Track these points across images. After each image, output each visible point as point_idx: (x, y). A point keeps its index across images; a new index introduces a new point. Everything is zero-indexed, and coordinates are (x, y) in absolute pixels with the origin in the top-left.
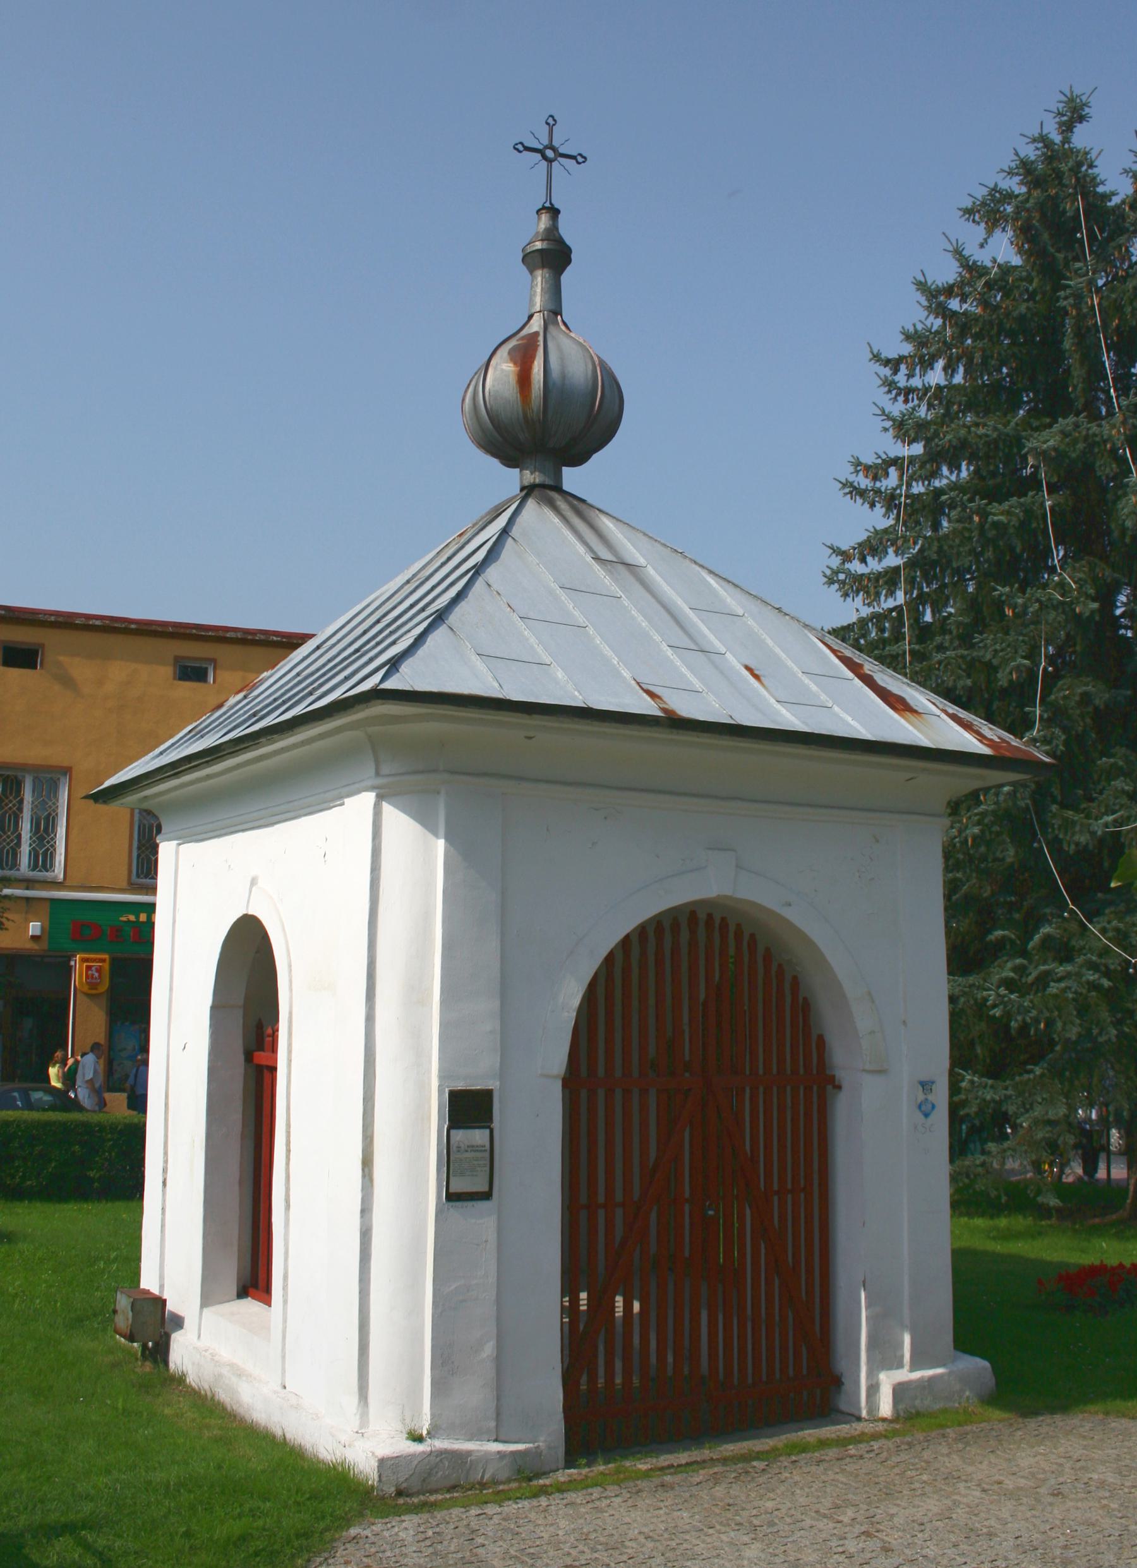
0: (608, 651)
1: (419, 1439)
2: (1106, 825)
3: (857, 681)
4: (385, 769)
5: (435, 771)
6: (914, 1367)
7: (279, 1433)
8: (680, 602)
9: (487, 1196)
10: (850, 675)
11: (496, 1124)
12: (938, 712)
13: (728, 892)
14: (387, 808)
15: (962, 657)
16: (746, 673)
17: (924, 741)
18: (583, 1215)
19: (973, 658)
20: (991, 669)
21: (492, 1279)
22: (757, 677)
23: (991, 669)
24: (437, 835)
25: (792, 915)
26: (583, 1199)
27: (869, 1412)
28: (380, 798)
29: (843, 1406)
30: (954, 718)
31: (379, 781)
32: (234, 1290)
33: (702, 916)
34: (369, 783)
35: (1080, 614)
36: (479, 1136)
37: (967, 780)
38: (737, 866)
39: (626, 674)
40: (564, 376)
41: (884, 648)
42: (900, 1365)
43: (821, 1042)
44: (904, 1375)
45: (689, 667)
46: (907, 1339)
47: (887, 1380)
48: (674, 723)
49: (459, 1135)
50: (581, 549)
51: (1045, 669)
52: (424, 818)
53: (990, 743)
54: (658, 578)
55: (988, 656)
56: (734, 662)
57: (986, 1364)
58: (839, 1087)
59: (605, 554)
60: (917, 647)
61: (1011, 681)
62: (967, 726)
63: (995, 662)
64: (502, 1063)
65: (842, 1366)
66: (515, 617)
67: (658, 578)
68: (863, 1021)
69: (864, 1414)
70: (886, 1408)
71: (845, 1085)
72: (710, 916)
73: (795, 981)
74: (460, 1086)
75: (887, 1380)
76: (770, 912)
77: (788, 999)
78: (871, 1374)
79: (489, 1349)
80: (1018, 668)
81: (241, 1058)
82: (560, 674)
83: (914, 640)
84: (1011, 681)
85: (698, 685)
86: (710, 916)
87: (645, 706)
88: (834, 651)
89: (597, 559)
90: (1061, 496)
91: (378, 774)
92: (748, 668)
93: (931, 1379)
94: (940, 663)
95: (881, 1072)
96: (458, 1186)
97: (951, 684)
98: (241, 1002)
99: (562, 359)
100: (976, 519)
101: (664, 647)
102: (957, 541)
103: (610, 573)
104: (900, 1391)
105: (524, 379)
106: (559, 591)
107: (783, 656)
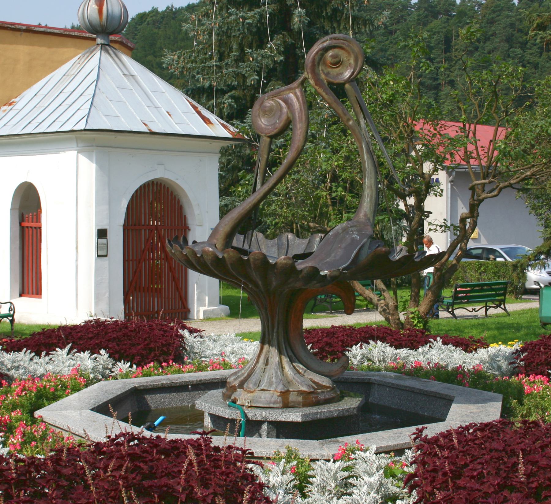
0: (132, 110)
1: (91, 316)
2: (281, 142)
3: (196, 114)
4: (80, 145)
5: (92, 146)
6: (209, 306)
7: (47, 324)
8: (148, 89)
9: (106, 256)
10: (194, 112)
11: (108, 238)
12: (218, 123)
13: (162, 176)
14: (79, 154)
15: (235, 72)
16: (167, 114)
17: (214, 135)
18: (127, 262)
19: (238, 73)
20: (244, 78)
21: (108, 277)
22: (170, 115)
23: (244, 78)
24: (93, 162)
25: (178, 182)
26: (127, 259)
27: (197, 318)
28: (78, 153)
29: (190, 317)
30: (223, 125)
31: (78, 148)
32: (18, 295)
33: (155, 183)
34: (76, 148)
35: (277, 61)
36: (104, 241)
37: (226, 144)
38: (165, 169)
39: (138, 118)
40: (112, 12)
41: (205, 63)
42: (205, 306)
43: (185, 216)
44: (206, 308)
45: (153, 113)
46: (207, 298)
47: (202, 309)
48: (152, 133)
49: (100, 240)
50: (120, 72)
51: (263, 81)
52: (90, 159)
53: (232, 133)
54: (141, 80)
55: (244, 73)
56: (164, 111)
57: (228, 307)
58: (190, 230)
59: (126, 73)
60: (218, 64)
61: (251, 84)
62: (225, 127)
63: (246, 75)
64: (109, 222)
65: (190, 306)
66: (108, 100)
67: (141, 80)
68: (196, 212)
69: (196, 318)
70: (201, 317)
71: (192, 229)
72: (157, 182)
73: (179, 200)
74: (100, 228)
75: (202, 309)
76: (171, 181)
77: (177, 206)
78: (197, 308)
79: (107, 295)
80: (253, 80)
81: (18, 224)
82: (123, 120)
83: (217, 60)
84: (251, 84)
85: (156, 120)
86: (157, 182)
87: (144, 129)
88: (190, 103)
89: (124, 74)
90: (273, 6)
91: (77, 146)
92: (168, 112)
93: (213, 310)
94: (226, 74)
95: (201, 225)
96: (100, 253)
97: (230, 83)
98: (18, 207)
99: (112, 8)
100: (241, 20)
101: (146, 107)
102: (235, 25)
103: (128, 79)
104: (205, 312)
105: (100, 11)
106: (117, 89)
107: (177, 107)
